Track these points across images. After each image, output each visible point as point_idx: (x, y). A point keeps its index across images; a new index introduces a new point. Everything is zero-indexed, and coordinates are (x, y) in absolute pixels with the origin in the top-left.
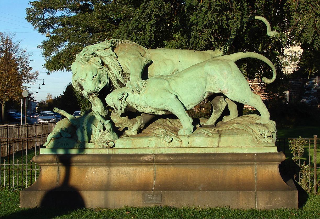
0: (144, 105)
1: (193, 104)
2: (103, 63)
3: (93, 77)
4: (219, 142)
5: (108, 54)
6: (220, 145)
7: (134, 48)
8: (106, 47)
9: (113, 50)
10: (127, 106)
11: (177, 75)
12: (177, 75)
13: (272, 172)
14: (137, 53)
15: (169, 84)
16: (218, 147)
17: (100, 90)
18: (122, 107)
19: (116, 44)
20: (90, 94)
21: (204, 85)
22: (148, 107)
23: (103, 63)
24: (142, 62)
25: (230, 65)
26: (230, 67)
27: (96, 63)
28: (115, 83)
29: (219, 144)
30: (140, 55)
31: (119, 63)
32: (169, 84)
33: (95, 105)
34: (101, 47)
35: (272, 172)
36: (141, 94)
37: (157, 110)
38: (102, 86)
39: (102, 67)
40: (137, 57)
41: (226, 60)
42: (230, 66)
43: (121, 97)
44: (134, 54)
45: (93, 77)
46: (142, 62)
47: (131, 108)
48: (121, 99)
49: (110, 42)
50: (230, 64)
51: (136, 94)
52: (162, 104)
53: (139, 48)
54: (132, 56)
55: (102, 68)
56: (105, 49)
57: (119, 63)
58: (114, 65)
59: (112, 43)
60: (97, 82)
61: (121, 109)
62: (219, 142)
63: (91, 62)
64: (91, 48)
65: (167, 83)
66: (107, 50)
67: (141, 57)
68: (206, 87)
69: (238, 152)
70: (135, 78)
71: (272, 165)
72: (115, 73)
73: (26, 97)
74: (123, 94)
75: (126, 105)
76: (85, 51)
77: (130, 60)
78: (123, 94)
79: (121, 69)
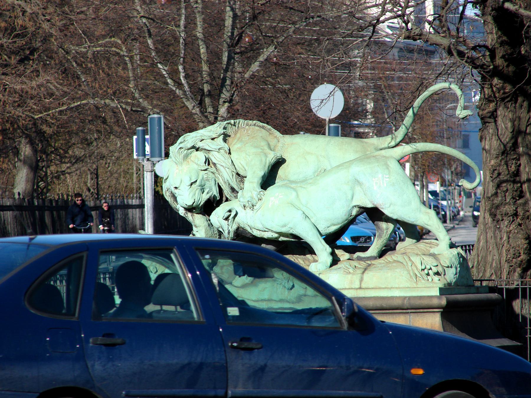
0: (260, 227)
1: (334, 225)
2: (208, 161)
3: (191, 185)
4: (361, 280)
5: (215, 147)
6: (363, 286)
7: (261, 135)
8: (214, 137)
9: (225, 140)
10: (238, 229)
11: (311, 181)
12: (311, 181)
13: (432, 324)
14: (263, 143)
15: (298, 195)
16: (360, 288)
17: (202, 204)
18: (229, 231)
19: (229, 131)
20: (190, 209)
21: (350, 197)
22: (266, 230)
23: (208, 161)
24: (266, 160)
25: (388, 165)
26: (388, 168)
27: (196, 162)
28: (227, 192)
29: (361, 284)
30: (266, 148)
31: (232, 162)
32: (298, 195)
33: (196, 227)
34: (207, 135)
35: (432, 324)
36: (255, 211)
37: (281, 234)
38: (205, 197)
39: (207, 167)
40: (261, 151)
41: (385, 157)
42: (387, 167)
43: (226, 216)
44: (256, 147)
45: (191, 185)
46: (266, 160)
47: (244, 230)
48: (227, 219)
49: (223, 127)
50: (389, 163)
51: (248, 210)
52: (285, 226)
53: (270, 134)
54: (254, 150)
55: (206, 170)
56: (213, 139)
57: (232, 162)
58: (223, 164)
59: (225, 128)
60: (197, 192)
61: (229, 233)
62: (361, 280)
63: (189, 161)
64: (189, 139)
65: (294, 194)
66: (216, 139)
67: (268, 151)
68: (354, 198)
69: (381, 295)
70: (251, 187)
71: (432, 314)
72: (226, 177)
73: (331, 121)
74: (230, 211)
75: (235, 227)
76: (181, 143)
77: (249, 155)
78: (230, 211)
79: (235, 171)
